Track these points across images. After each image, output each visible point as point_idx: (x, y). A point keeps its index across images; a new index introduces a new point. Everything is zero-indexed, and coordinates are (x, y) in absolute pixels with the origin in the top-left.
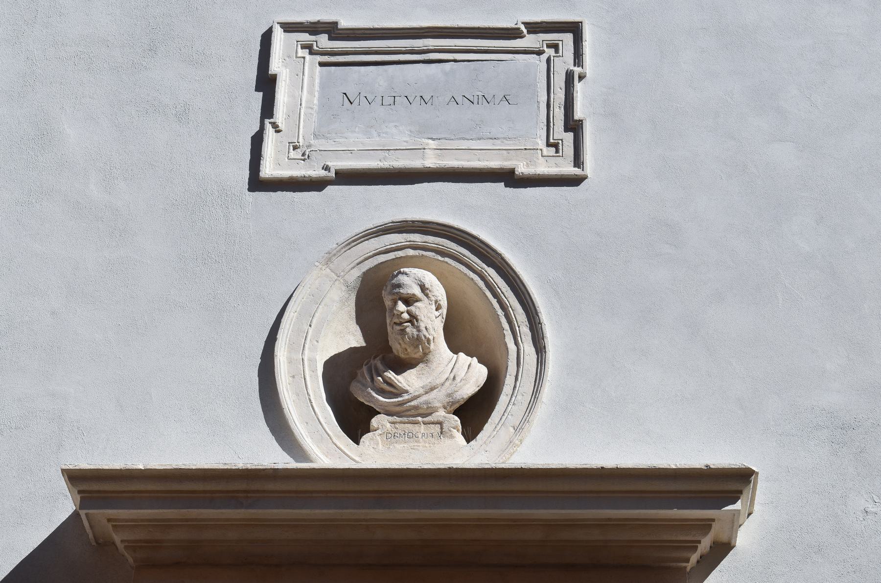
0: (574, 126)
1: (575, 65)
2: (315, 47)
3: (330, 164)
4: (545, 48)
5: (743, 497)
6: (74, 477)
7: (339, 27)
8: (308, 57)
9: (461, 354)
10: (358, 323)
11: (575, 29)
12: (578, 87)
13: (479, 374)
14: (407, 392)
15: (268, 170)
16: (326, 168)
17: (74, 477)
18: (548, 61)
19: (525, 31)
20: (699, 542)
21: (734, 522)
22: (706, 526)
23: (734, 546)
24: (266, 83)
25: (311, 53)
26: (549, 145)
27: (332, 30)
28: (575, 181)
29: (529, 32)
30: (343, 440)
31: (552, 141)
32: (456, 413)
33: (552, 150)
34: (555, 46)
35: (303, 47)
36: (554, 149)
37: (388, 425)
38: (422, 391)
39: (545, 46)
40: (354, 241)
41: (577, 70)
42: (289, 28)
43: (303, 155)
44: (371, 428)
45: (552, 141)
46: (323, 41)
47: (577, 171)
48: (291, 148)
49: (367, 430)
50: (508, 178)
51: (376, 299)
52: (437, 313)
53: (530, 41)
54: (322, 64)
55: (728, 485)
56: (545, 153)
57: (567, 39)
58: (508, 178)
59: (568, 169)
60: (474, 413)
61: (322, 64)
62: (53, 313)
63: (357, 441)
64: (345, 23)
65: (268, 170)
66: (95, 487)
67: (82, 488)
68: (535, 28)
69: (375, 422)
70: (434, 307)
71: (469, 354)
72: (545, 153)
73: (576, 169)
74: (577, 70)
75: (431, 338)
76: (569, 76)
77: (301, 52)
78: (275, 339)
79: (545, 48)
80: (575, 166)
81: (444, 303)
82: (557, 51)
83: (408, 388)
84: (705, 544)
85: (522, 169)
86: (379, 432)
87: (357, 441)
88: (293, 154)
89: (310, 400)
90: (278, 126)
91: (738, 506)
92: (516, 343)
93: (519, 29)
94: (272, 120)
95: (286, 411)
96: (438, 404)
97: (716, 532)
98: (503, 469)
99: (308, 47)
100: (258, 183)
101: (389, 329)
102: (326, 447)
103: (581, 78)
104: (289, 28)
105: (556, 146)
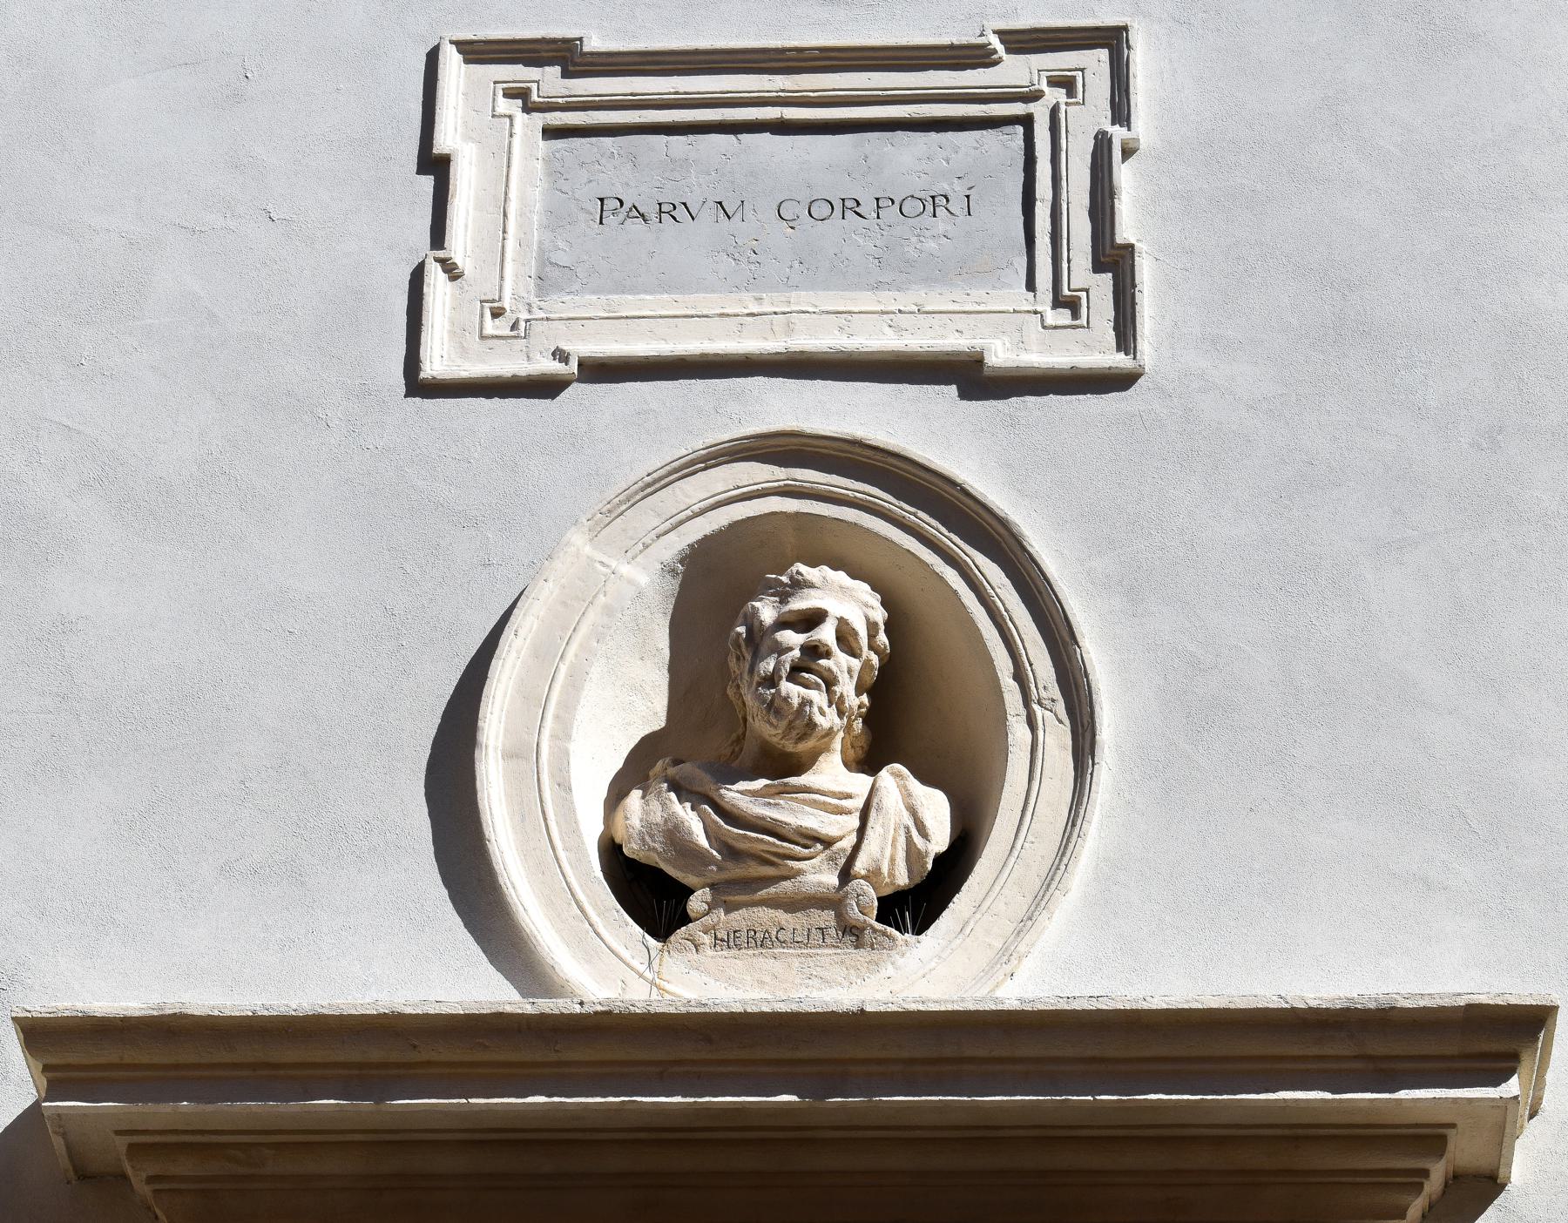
0: (1114, 259)
1: (1113, 123)
2: (535, 97)
3: (566, 347)
4: (1044, 86)
5: (1527, 1064)
6: (38, 1035)
7: (558, 69)
8: (520, 117)
10: (670, 670)
11: (1112, 39)
12: (1124, 175)
15: (434, 365)
16: (561, 356)
17: (38, 1035)
18: (1054, 111)
19: (1000, 48)
20: (1425, 1173)
21: (1501, 1126)
22: (1429, 1137)
23: (1502, 1187)
24: (435, 165)
25: (528, 108)
26: (1058, 302)
27: (567, 56)
28: (1119, 381)
29: (1009, 51)
31: (1066, 292)
33: (1064, 317)
34: (1066, 83)
35: (509, 94)
36: (1067, 312)
39: (1045, 81)
40: (676, 471)
41: (1118, 133)
42: (475, 52)
43: (514, 327)
45: (1066, 292)
46: (548, 81)
47: (1121, 361)
48: (488, 314)
49: (685, 919)
50: (970, 377)
51: (718, 601)
53: (1015, 70)
54: (551, 133)
55: (1497, 1038)
56: (1049, 321)
57: (1096, 61)
58: (970, 377)
59: (1103, 356)
61: (551, 133)
62: (390, 248)
64: (595, 43)
65: (434, 365)
66: (58, 1074)
67: (53, 1060)
68: (1024, 42)
72: (1049, 321)
73: (1122, 355)
74: (1118, 133)
76: (1102, 144)
77: (504, 106)
79: (1044, 86)
80: (1119, 349)
82: (1071, 93)
84: (1438, 1172)
85: (1001, 355)
88: (490, 327)
90: (455, 266)
91: (1512, 1087)
93: (983, 46)
94: (441, 254)
95: (503, 880)
97: (1464, 1151)
99: (519, 94)
100: (418, 386)
102: (602, 964)
103: (1128, 153)
104: (475, 52)
105: (1072, 305)
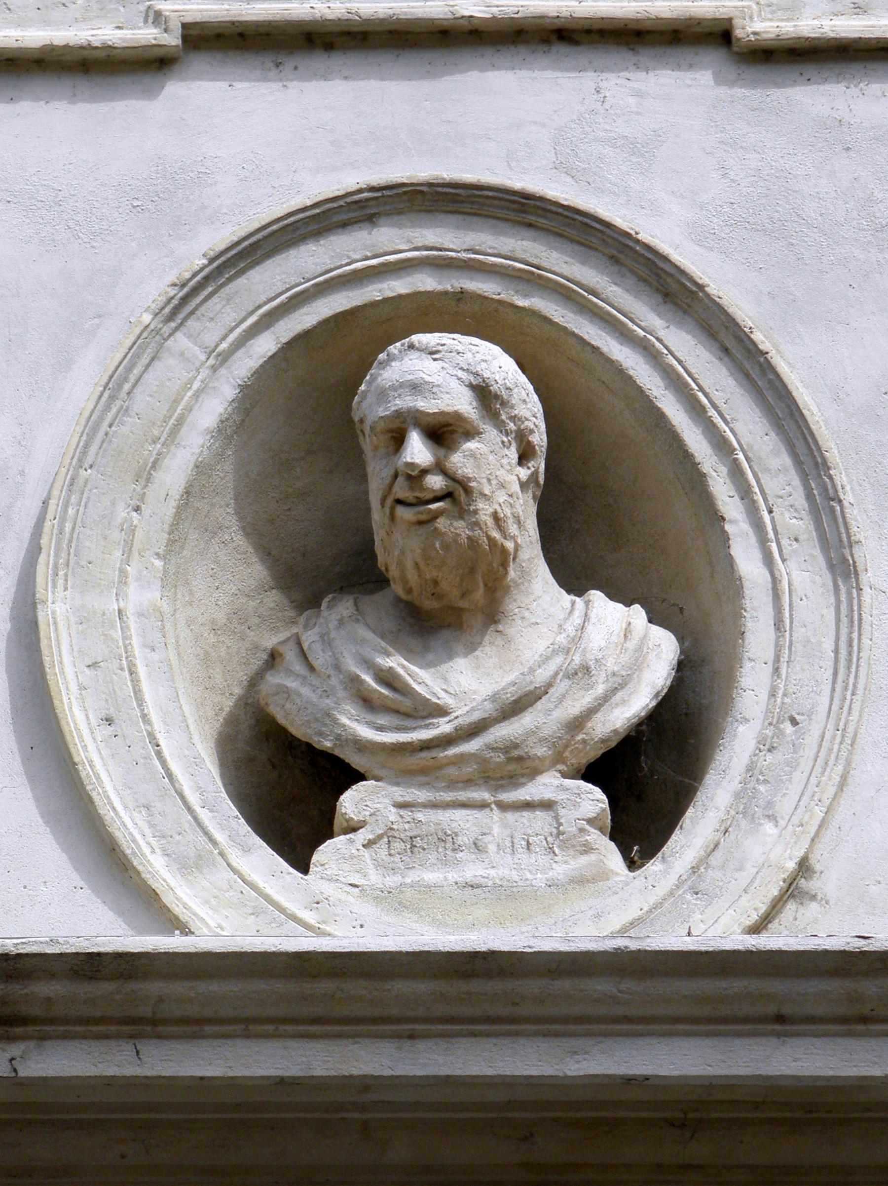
9: (597, 596)
13: (662, 650)
14: (442, 711)
16: (157, 18)
30: (262, 862)
32: (592, 773)
37: (392, 814)
38: (488, 709)
44: (338, 822)
52: (524, 473)
60: (645, 780)
63: (301, 862)
69: (351, 802)
70: (513, 454)
71: (621, 594)
75: (510, 545)
78: (777, 424)
81: (540, 439)
83: (446, 700)
86: (362, 836)
87: (303, 867)
89: (151, 735)
92: (768, 561)
96: (541, 751)
98: (780, 952)
101: (377, 516)
102: (234, 897)
